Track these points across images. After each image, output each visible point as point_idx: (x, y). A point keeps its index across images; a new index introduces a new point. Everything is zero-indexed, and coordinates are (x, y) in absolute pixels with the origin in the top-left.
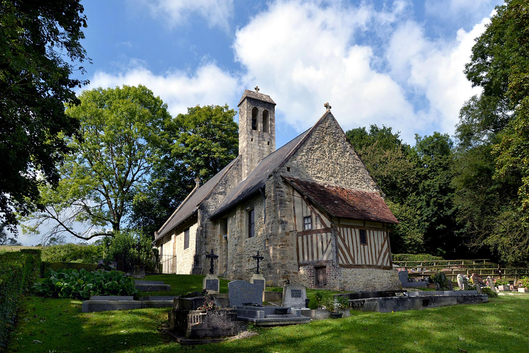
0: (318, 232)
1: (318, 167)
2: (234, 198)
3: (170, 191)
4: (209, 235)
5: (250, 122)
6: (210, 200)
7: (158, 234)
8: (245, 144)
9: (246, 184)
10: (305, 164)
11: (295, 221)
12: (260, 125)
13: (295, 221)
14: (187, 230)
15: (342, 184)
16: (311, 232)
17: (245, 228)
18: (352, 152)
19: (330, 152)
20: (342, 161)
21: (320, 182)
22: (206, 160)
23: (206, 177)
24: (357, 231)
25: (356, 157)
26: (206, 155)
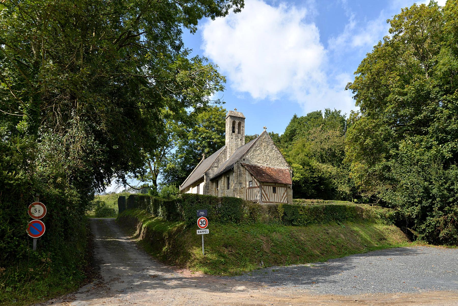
0: (256, 187)
1: (258, 158)
2: (222, 170)
3: (187, 160)
4: (210, 188)
5: (231, 129)
6: (210, 170)
7: (181, 187)
8: (228, 141)
9: (228, 163)
10: (252, 157)
11: (37, 230)
12: (236, 130)
13: (37, 230)
14: (198, 185)
15: (270, 166)
16: (252, 188)
17: (226, 185)
18: (276, 149)
19: (265, 150)
20: (270, 154)
21: (259, 165)
22: (209, 143)
23: (209, 153)
24: (272, 187)
25: (278, 152)
26: (209, 140)
